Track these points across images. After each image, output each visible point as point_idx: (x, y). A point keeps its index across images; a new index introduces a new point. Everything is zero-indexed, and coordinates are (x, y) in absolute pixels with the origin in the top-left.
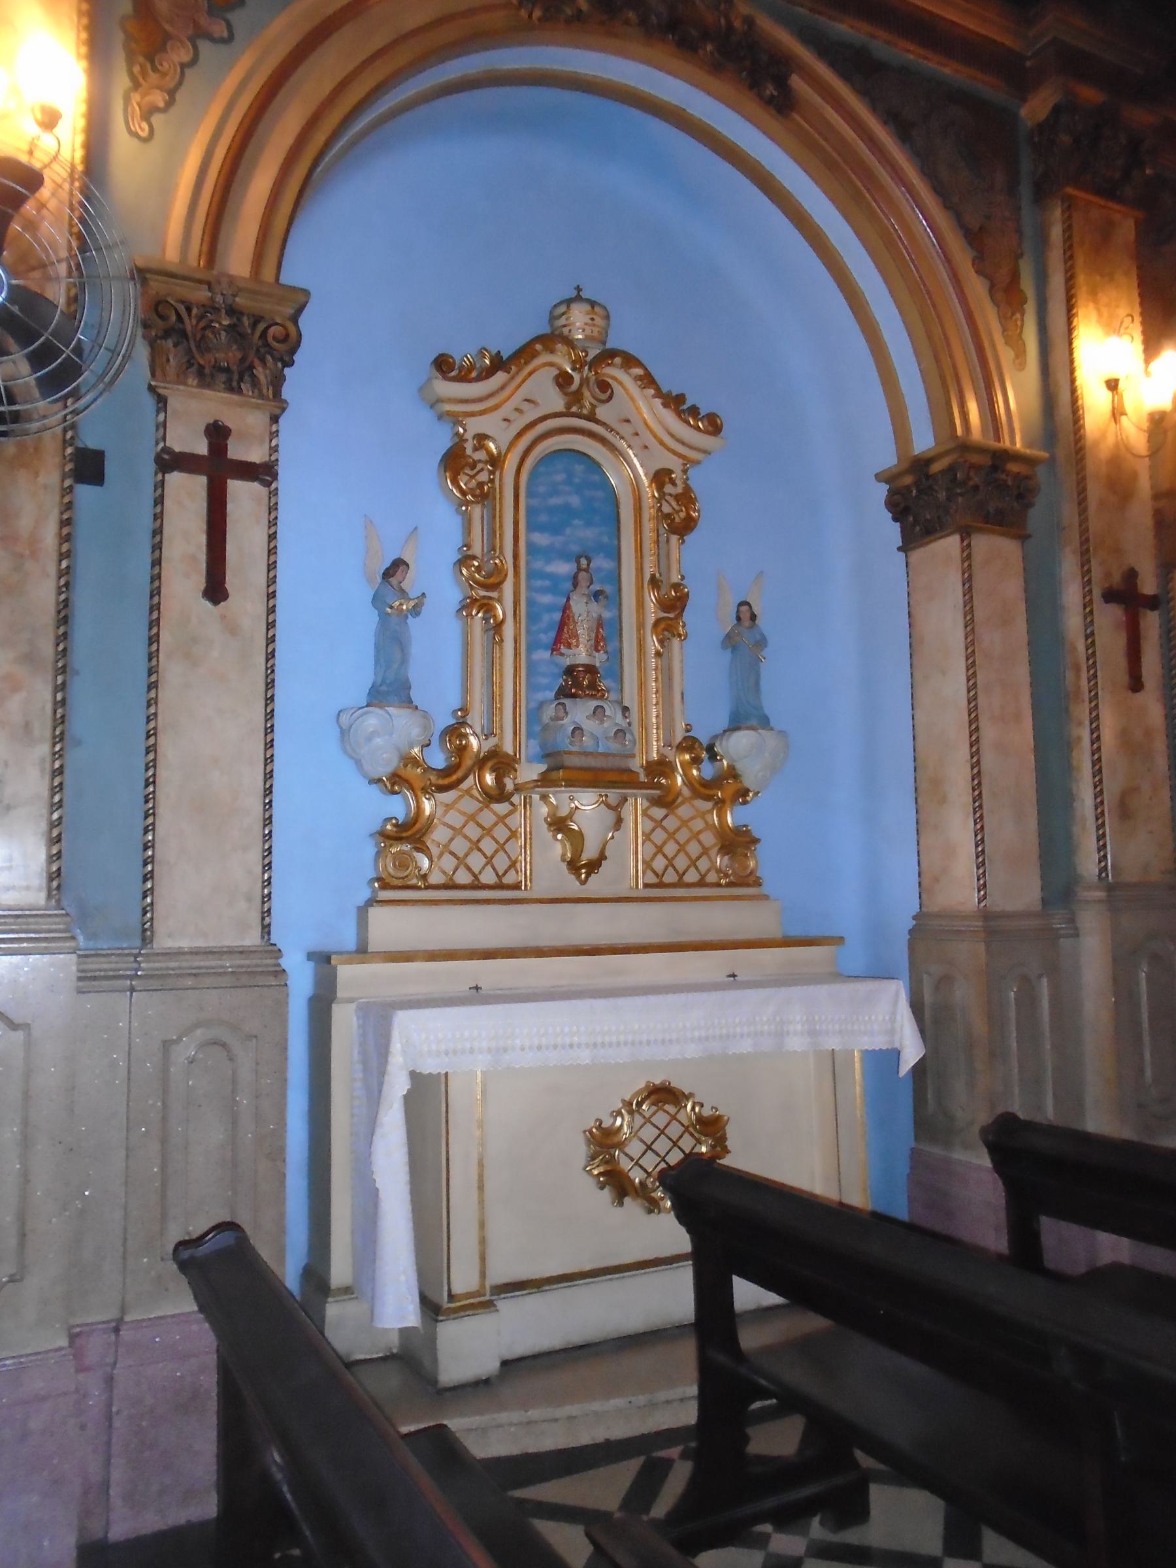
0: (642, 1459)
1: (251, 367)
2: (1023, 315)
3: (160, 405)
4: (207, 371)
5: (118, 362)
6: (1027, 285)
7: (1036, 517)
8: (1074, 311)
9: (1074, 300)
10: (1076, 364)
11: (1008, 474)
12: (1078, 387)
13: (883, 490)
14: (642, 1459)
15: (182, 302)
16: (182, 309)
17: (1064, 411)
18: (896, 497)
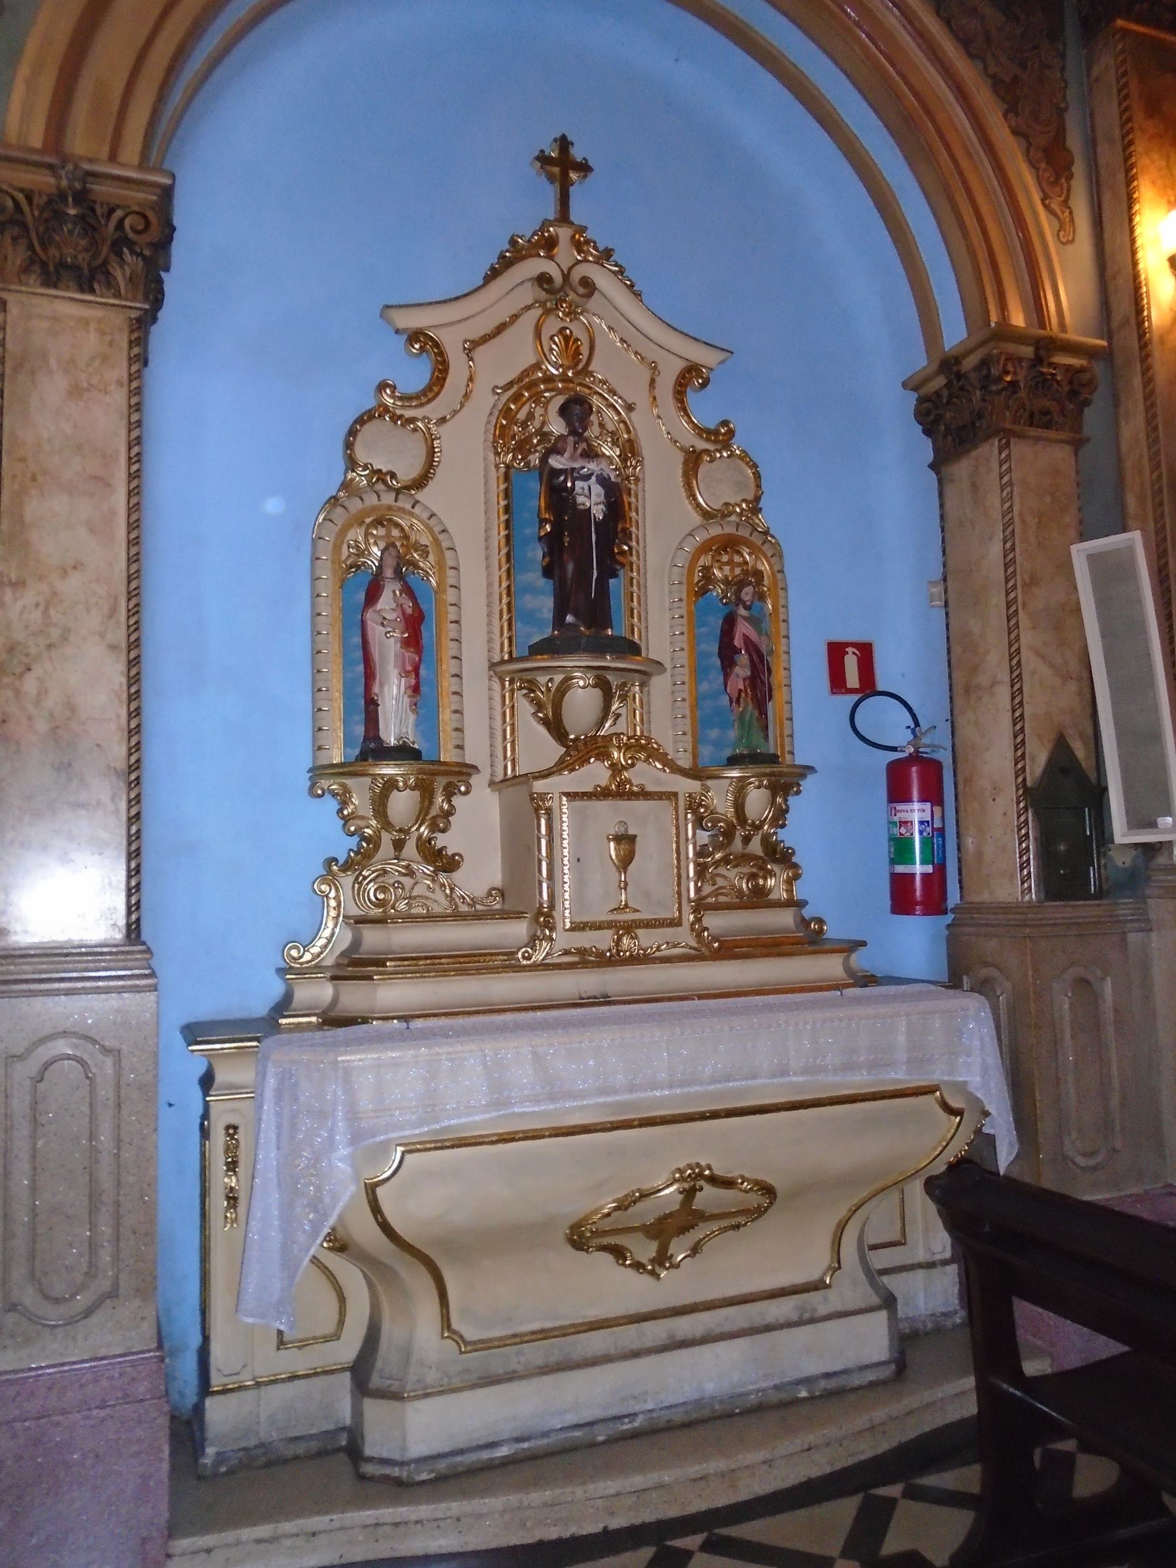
0: (705, 1535)
1: (105, 263)
2: (1070, 177)
3: (704, 686)
4: (52, 268)
5: (1127, 901)
6: (1074, 141)
7: (1093, 418)
8: (1135, 196)
9: (1135, 183)
10: (1139, 243)
11: (1055, 366)
12: (1141, 272)
13: (911, 398)
14: (705, 1535)
15: (22, 190)
16: (20, 197)
17: (1122, 308)
18: (926, 405)
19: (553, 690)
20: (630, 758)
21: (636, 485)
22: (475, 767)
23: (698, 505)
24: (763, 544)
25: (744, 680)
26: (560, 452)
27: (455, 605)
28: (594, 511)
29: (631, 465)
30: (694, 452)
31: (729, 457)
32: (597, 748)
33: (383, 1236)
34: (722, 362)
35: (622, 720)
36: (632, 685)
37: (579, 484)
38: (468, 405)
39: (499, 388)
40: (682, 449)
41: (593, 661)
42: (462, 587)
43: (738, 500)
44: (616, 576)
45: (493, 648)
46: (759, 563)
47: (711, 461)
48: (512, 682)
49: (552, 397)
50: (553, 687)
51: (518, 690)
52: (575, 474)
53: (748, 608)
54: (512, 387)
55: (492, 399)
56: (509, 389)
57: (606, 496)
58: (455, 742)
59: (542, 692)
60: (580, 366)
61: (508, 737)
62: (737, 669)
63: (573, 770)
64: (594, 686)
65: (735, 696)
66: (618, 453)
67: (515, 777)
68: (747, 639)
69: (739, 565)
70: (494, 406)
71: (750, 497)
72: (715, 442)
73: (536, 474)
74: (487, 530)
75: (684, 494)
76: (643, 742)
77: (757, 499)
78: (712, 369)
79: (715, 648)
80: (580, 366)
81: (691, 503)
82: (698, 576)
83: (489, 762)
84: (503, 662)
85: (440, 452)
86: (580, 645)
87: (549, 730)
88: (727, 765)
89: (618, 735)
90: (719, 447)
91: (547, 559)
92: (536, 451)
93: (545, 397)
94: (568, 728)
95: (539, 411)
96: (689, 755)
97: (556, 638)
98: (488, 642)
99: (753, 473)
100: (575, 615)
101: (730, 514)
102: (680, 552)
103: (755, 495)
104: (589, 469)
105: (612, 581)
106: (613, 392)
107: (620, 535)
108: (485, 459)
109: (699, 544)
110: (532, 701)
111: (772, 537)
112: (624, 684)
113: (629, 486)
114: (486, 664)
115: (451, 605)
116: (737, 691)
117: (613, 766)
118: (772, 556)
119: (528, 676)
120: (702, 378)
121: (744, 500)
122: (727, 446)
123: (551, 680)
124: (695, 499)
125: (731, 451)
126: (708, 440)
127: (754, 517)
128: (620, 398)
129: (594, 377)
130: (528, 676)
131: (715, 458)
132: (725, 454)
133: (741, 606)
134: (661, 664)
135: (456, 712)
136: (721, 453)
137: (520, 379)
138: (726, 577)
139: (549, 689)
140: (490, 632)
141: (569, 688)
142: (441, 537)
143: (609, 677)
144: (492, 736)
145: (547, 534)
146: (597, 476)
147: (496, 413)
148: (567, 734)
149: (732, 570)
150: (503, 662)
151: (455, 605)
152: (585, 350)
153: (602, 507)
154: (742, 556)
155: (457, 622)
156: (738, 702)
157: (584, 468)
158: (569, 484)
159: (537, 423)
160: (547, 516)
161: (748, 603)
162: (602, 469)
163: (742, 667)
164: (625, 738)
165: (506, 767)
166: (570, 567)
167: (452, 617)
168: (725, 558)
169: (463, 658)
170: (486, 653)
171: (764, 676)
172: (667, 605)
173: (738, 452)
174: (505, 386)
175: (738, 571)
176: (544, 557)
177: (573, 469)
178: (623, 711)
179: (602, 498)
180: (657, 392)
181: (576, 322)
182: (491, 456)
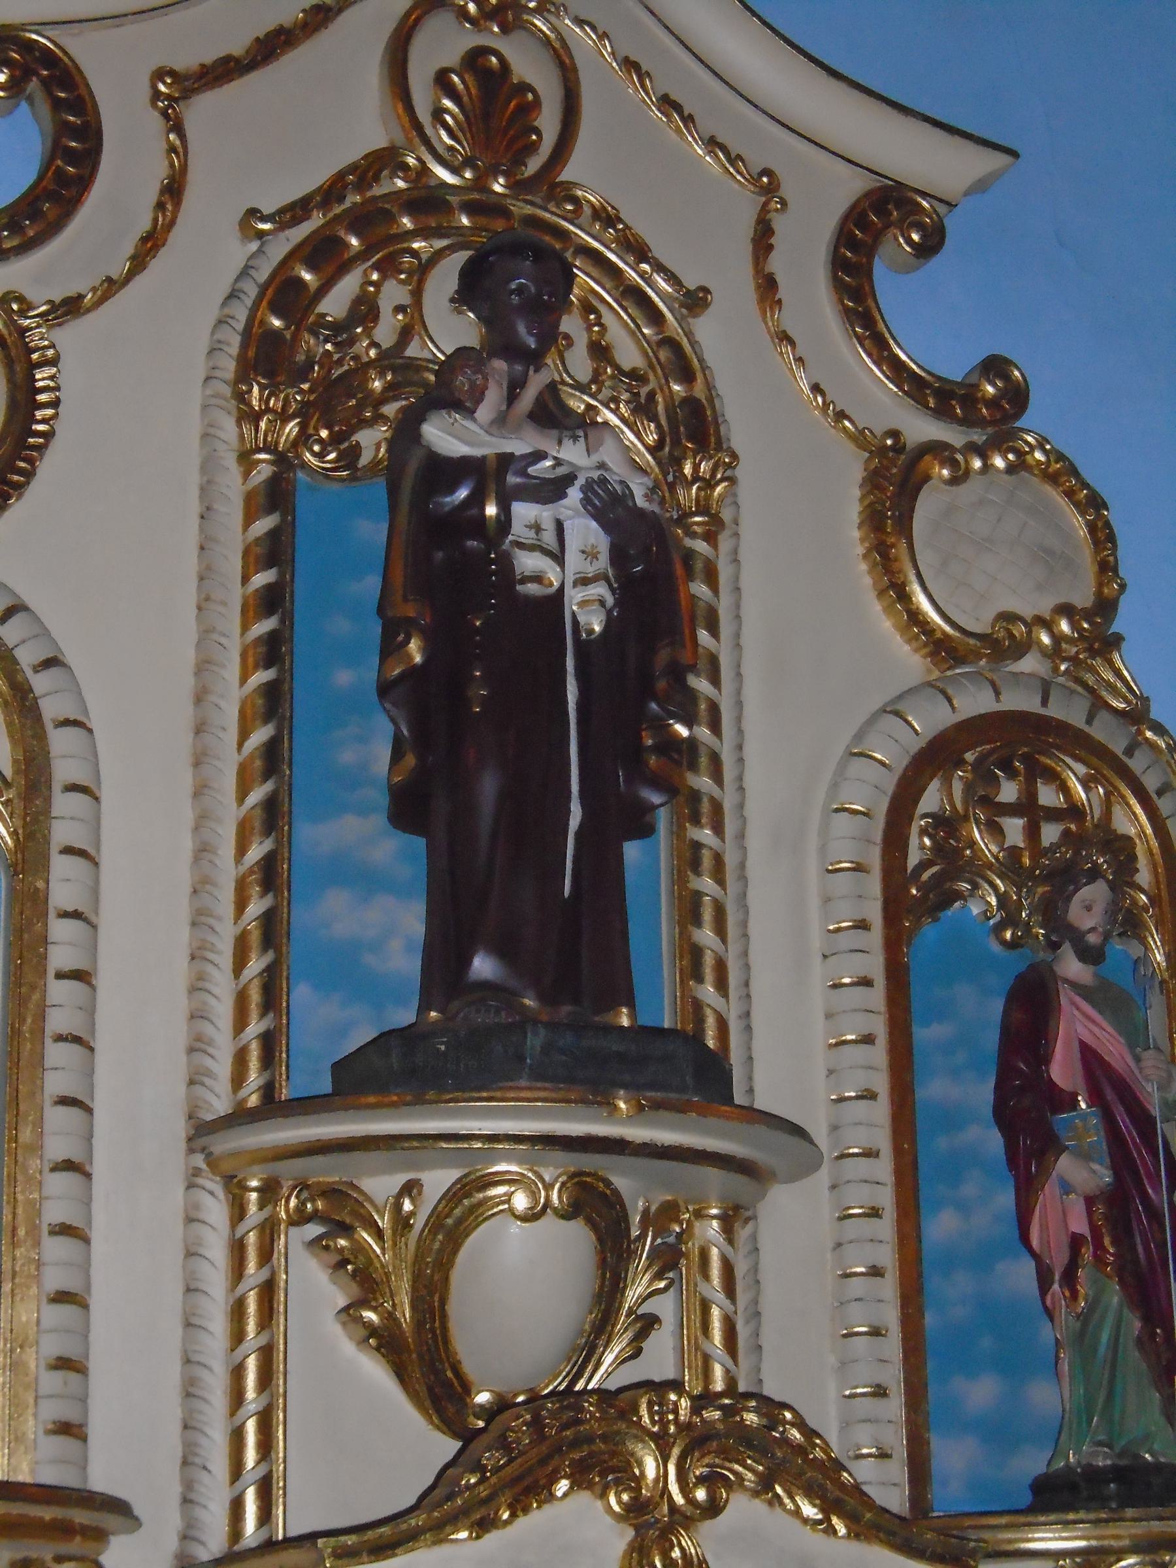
19: (419, 1222)
20: (701, 1480)
21: (710, 537)
22: (119, 1507)
23: (915, 617)
24: (1129, 752)
25: (1090, 1201)
26: (463, 405)
27: (76, 915)
28: (574, 598)
29: (696, 478)
30: (899, 448)
31: (1011, 469)
32: (575, 1444)
33: (572, 159)
34: (980, 186)
35: (660, 1344)
36: (699, 1214)
37: (524, 512)
38: (157, 265)
39: (264, 219)
40: (859, 438)
41: (566, 1118)
42: (107, 857)
43: (1044, 607)
44: (645, 831)
45: (209, 1073)
46: (1118, 812)
47: (954, 481)
48: (269, 1191)
49: (438, 256)
50: (420, 1211)
51: (292, 1223)
52: (512, 479)
53: (1091, 955)
54: (306, 217)
55: (240, 251)
56: (296, 221)
57: (618, 556)
58: (53, 1411)
59: (379, 1234)
60: (533, 165)
61: (250, 1394)
62: (1065, 1165)
63: (483, 1526)
64: (566, 1215)
65: (1059, 1260)
66: (651, 438)
67: (269, 1546)
68: (1090, 1057)
69: (1054, 814)
70: (245, 273)
71: (1083, 598)
72: (968, 422)
73: (378, 489)
74: (204, 666)
75: (868, 581)
76: (751, 1418)
77: (1105, 607)
78: (951, 205)
79: (983, 1093)
80: (533, 165)
81: (889, 610)
82: (919, 846)
83: (177, 1489)
84: (240, 1117)
85: (55, 404)
86: (521, 1058)
87: (401, 1373)
88: (1031, 1510)
89: (657, 1388)
90: (978, 436)
91: (410, 760)
92: (378, 418)
93: (415, 253)
94: (469, 1368)
95: (393, 293)
96: (898, 1470)
97: (435, 1031)
98: (191, 1050)
99: (1092, 528)
100: (504, 951)
101: (1020, 648)
102: (858, 767)
103: (1099, 594)
104: (558, 462)
105: (632, 851)
106: (638, 251)
107: (661, 684)
108: (205, 436)
109: (921, 743)
110: (343, 1263)
111: (1159, 729)
112: (670, 1211)
113: (688, 542)
114: (180, 1129)
115: (65, 915)
116: (1065, 1241)
117: (637, 1510)
118: (1160, 793)
119: (326, 1171)
120: (920, 227)
121: (1066, 610)
122: (1003, 439)
123: (410, 1189)
124: (904, 597)
125: (1019, 453)
126: (942, 412)
127: (1097, 662)
128: (660, 268)
129: (575, 200)
130: (326, 1171)
131: (968, 471)
132: (999, 462)
133: (1067, 950)
134: (798, 1131)
135: (62, 1297)
136: (984, 457)
137: (331, 192)
138: (1014, 853)
139: (402, 1223)
140: (197, 1016)
141: (476, 1215)
142: (40, 683)
143: (621, 1182)
144: (190, 1391)
145: (413, 672)
146: (588, 488)
147: (251, 291)
148: (467, 1389)
149: (1033, 833)
150: (240, 1117)
151: (76, 915)
152: (548, 123)
153: (600, 590)
154: (1064, 788)
155: (80, 976)
156: (1069, 1278)
157: (539, 456)
158: (491, 510)
159: (386, 331)
160: (410, 611)
161: (1092, 939)
162: (602, 466)
163: (1085, 1156)
164: (684, 1403)
165: (237, 1506)
166: (488, 787)
167: (57, 1148)
168: (1009, 792)
169: (99, 1045)
170: (182, 1089)
171: (1157, 1187)
172: (816, 943)
173: (1038, 455)
174: (281, 211)
175: (1050, 833)
176: (397, 755)
177: (505, 461)
178: (665, 1307)
179: (603, 562)
180: (776, 264)
181: (518, 36)
182: (228, 428)
